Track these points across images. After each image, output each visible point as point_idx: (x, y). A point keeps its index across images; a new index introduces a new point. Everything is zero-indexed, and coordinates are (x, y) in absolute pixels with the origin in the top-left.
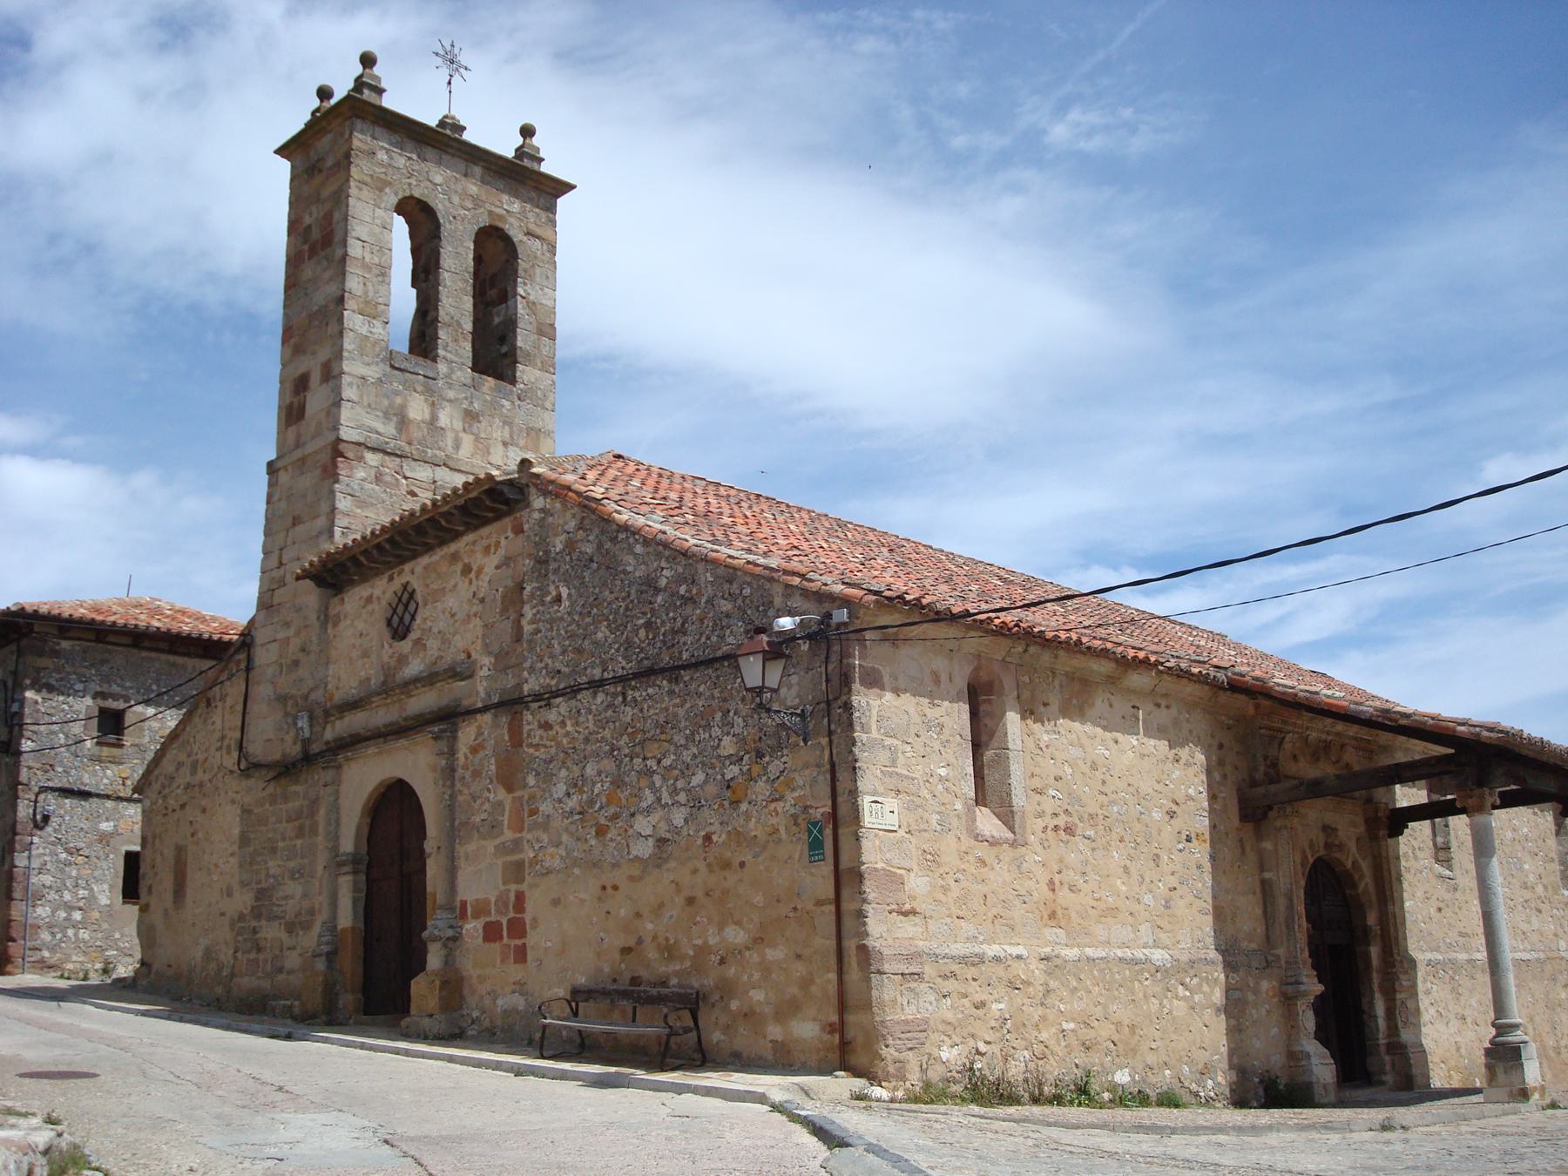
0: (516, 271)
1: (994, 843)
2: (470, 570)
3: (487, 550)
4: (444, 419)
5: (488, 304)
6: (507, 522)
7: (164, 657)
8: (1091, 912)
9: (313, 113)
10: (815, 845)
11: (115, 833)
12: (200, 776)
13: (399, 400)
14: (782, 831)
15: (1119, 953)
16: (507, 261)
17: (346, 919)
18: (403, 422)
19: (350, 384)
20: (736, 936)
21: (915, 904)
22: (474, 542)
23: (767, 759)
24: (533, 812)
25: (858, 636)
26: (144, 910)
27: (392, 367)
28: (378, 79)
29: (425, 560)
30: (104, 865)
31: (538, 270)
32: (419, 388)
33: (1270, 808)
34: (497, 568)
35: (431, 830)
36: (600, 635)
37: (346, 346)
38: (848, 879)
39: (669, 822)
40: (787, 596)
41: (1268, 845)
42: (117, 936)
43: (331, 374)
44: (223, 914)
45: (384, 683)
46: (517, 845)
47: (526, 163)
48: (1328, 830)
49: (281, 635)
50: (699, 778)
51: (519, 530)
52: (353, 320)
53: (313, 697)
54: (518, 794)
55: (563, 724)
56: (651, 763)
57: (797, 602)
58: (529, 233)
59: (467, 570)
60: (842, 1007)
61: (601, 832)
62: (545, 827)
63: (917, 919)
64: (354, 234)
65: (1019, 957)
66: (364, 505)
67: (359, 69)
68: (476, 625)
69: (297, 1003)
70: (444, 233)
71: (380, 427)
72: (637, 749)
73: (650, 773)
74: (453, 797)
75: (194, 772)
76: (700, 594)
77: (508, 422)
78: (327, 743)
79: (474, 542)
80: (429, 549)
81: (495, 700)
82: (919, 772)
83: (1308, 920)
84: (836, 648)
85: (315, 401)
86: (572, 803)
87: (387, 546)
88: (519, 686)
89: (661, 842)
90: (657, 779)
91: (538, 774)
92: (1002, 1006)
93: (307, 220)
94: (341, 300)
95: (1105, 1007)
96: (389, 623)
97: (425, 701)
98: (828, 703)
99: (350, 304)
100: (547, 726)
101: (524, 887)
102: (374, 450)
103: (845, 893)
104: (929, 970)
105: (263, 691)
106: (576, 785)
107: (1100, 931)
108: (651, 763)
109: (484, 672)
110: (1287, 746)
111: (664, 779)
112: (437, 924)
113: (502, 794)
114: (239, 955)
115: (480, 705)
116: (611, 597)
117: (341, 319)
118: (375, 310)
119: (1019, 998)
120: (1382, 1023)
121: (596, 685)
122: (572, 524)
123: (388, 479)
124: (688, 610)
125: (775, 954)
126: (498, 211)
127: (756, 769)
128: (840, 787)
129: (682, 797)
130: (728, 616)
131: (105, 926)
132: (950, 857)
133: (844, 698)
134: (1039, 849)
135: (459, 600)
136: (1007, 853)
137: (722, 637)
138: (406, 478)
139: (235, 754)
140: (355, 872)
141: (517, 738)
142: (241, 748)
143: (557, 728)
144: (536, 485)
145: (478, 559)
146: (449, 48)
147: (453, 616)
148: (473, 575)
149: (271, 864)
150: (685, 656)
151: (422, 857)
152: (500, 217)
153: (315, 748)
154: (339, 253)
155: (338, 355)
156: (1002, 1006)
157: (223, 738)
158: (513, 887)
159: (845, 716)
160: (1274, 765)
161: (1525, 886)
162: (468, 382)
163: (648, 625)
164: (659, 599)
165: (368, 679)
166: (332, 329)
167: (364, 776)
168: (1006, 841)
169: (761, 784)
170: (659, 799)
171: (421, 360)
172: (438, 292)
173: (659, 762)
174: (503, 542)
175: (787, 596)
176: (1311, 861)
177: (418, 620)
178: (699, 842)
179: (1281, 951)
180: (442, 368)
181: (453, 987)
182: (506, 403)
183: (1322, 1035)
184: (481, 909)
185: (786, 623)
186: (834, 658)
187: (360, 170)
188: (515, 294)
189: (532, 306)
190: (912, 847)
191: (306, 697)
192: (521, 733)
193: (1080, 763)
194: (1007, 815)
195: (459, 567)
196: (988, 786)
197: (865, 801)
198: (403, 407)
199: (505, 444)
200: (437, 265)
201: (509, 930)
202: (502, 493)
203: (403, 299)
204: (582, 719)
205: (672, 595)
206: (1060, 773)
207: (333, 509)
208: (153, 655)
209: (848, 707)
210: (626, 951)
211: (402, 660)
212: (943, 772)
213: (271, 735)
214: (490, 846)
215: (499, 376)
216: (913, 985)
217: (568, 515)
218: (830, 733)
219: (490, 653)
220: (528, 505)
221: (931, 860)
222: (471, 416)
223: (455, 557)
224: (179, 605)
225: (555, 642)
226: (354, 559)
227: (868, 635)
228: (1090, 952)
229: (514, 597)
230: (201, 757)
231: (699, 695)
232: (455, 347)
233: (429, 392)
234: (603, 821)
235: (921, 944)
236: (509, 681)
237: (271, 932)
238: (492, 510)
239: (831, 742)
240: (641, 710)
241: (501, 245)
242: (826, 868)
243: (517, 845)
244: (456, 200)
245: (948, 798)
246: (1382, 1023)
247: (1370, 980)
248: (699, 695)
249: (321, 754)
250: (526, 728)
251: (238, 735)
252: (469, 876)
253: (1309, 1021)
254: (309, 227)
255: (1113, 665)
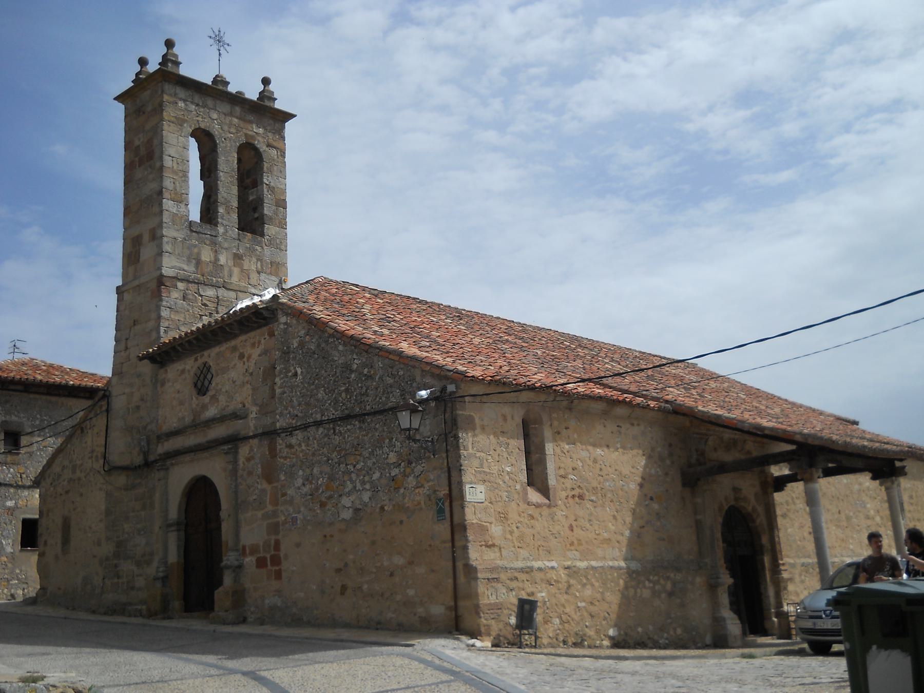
0: (263, 168)
1: (538, 506)
2: (244, 357)
3: (253, 345)
4: (223, 259)
5: (246, 188)
6: (265, 329)
7: (44, 397)
8: (595, 541)
9: (137, 75)
10: (441, 511)
11: (17, 507)
12: (78, 474)
13: (196, 250)
14: (422, 502)
15: (611, 563)
16: (257, 163)
17: (173, 556)
18: (198, 262)
19: (167, 243)
20: (399, 560)
21: (494, 541)
22: (246, 341)
23: (414, 465)
24: (284, 495)
25: (460, 399)
26: (41, 555)
27: (192, 231)
28: (176, 56)
29: (216, 350)
30: (9, 527)
31: (275, 168)
32: (208, 242)
33: (699, 479)
34: (259, 355)
35: (224, 505)
36: (320, 395)
37: (164, 220)
38: (458, 529)
39: (361, 499)
40: (423, 376)
41: (699, 500)
42: (18, 571)
43: (156, 236)
44: (94, 556)
45: (193, 421)
46: (275, 514)
47: (267, 103)
48: (736, 490)
49: (127, 390)
50: (376, 476)
51: (272, 334)
52: (168, 204)
53: (149, 427)
54: (275, 484)
55: (300, 445)
56: (350, 467)
57: (428, 380)
58: (269, 146)
59: (241, 356)
60: (456, 598)
61: (323, 505)
62: (291, 502)
63: (496, 549)
64: (167, 153)
65: (553, 568)
66: (179, 317)
67: (164, 50)
68: (247, 390)
69: (144, 607)
70: (220, 150)
71: (186, 267)
72: (342, 459)
73: (350, 473)
74: (236, 486)
75: (74, 472)
76: (375, 374)
77: (259, 259)
78: (160, 455)
79: (246, 341)
80: (219, 343)
81: (260, 431)
82: (495, 469)
83: (724, 542)
84: (450, 405)
85: (147, 252)
86: (305, 490)
87: (194, 342)
88: (274, 423)
89: (357, 510)
90: (354, 476)
91: (286, 473)
92: (544, 594)
93: (137, 143)
94: (160, 193)
95: (602, 593)
96: (195, 385)
97: (219, 431)
98: (446, 435)
99: (166, 194)
100: (290, 446)
101: (280, 537)
102: (182, 280)
103: (457, 537)
104: (503, 577)
105: (117, 423)
106: (308, 480)
107: (600, 553)
108: (350, 467)
109: (253, 415)
110: (710, 443)
111: (358, 475)
112: (229, 558)
113: (265, 485)
114: (106, 580)
115: (251, 434)
116: (325, 374)
117: (161, 204)
118: (181, 199)
119: (553, 590)
120: (772, 600)
121: (318, 424)
122: (302, 333)
123: (190, 297)
124: (369, 383)
125: (421, 570)
126: (250, 133)
127: (408, 470)
128: (453, 480)
129: (368, 486)
130: (391, 387)
131: (10, 565)
132: (513, 516)
133: (454, 432)
134: (563, 507)
135: (237, 375)
136: (545, 511)
137: (388, 398)
138: (201, 296)
139: (101, 461)
140: (178, 530)
141: (273, 452)
142: (105, 458)
143: (296, 447)
144: (282, 309)
145: (248, 351)
146: (222, 48)
147: (234, 382)
148: (245, 359)
149: (126, 526)
150: (368, 408)
151: (218, 520)
152: (252, 137)
153: (152, 458)
154: (158, 164)
155: (160, 225)
156: (544, 594)
157: (93, 451)
158: (273, 537)
159: (455, 442)
160: (703, 454)
161: (868, 517)
162: (236, 236)
163: (347, 391)
164: (353, 376)
165: (183, 418)
166: (156, 209)
167: (181, 476)
168: (545, 505)
169: (411, 478)
170: (355, 487)
171: (208, 226)
172: (217, 184)
173: (355, 467)
174: (263, 341)
175: (423, 376)
176: (726, 508)
177: (213, 385)
178: (378, 510)
179: (707, 560)
180: (221, 230)
181: (239, 597)
182: (258, 248)
183: (735, 607)
184: (254, 550)
185: (424, 393)
186: (448, 410)
187: (169, 113)
188: (262, 183)
189: (272, 189)
190: (492, 510)
191: (145, 428)
192: (275, 449)
193: (587, 459)
194: (545, 491)
195: (237, 354)
196: (536, 477)
197: (467, 487)
198: (199, 254)
199: (259, 273)
200: (216, 169)
201: (271, 561)
202: (262, 314)
203: (196, 189)
204: (310, 443)
205: (360, 374)
206: (574, 466)
207: (159, 317)
208: (37, 396)
209: (456, 438)
210: (338, 570)
211: (204, 407)
212: (508, 469)
213: (123, 450)
214: (259, 514)
215: (253, 232)
216: (494, 584)
217: (300, 328)
218: (447, 451)
219: (256, 405)
220: (277, 321)
221: (503, 517)
222: (238, 257)
223: (235, 349)
224: (49, 361)
225: (294, 399)
226: (174, 348)
227: (467, 399)
228: (594, 563)
229: (270, 372)
230: (79, 462)
231: (376, 429)
232: (228, 218)
233: (214, 244)
234: (323, 499)
235: (499, 563)
236: (268, 420)
237: (126, 567)
238: (256, 322)
239: (447, 456)
240: (344, 438)
241: (253, 153)
242: (447, 524)
243: (275, 514)
244: (226, 128)
245: (511, 483)
246: (772, 600)
247: (765, 575)
248: (376, 429)
249: (156, 461)
250: (279, 447)
251: (103, 449)
252: (245, 531)
253: (725, 599)
254: (139, 146)
255: (605, 404)
